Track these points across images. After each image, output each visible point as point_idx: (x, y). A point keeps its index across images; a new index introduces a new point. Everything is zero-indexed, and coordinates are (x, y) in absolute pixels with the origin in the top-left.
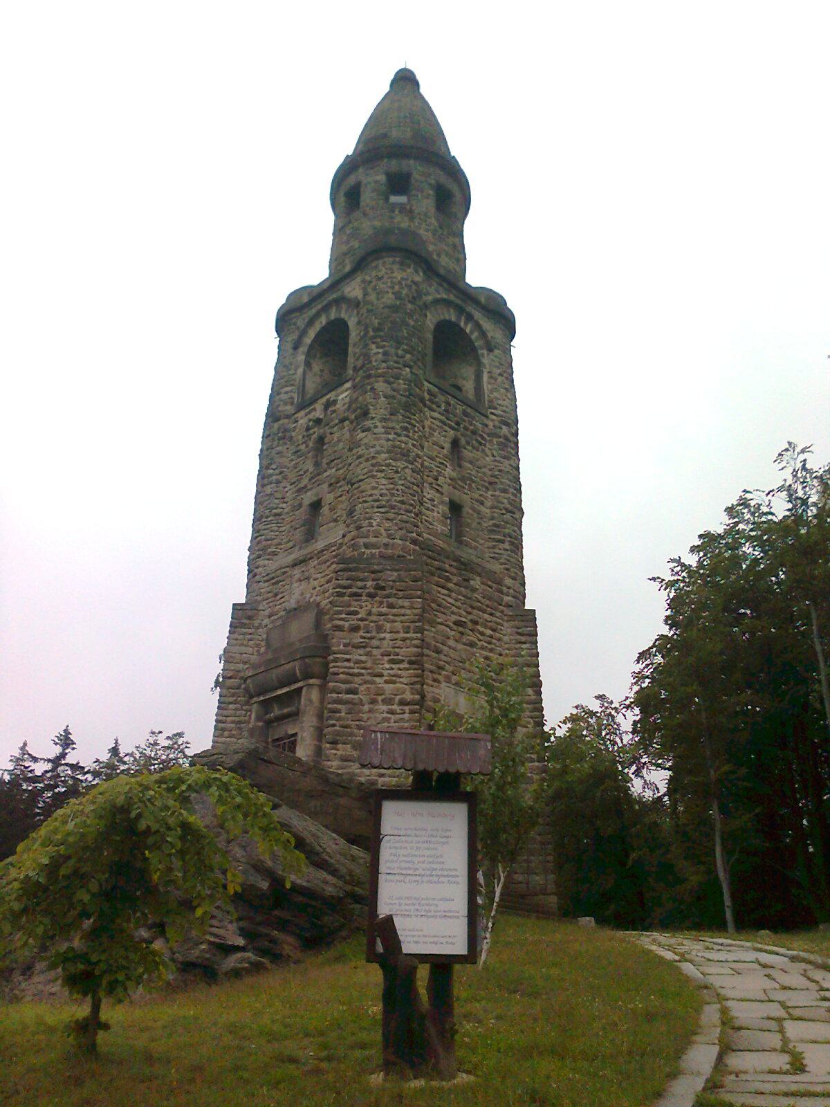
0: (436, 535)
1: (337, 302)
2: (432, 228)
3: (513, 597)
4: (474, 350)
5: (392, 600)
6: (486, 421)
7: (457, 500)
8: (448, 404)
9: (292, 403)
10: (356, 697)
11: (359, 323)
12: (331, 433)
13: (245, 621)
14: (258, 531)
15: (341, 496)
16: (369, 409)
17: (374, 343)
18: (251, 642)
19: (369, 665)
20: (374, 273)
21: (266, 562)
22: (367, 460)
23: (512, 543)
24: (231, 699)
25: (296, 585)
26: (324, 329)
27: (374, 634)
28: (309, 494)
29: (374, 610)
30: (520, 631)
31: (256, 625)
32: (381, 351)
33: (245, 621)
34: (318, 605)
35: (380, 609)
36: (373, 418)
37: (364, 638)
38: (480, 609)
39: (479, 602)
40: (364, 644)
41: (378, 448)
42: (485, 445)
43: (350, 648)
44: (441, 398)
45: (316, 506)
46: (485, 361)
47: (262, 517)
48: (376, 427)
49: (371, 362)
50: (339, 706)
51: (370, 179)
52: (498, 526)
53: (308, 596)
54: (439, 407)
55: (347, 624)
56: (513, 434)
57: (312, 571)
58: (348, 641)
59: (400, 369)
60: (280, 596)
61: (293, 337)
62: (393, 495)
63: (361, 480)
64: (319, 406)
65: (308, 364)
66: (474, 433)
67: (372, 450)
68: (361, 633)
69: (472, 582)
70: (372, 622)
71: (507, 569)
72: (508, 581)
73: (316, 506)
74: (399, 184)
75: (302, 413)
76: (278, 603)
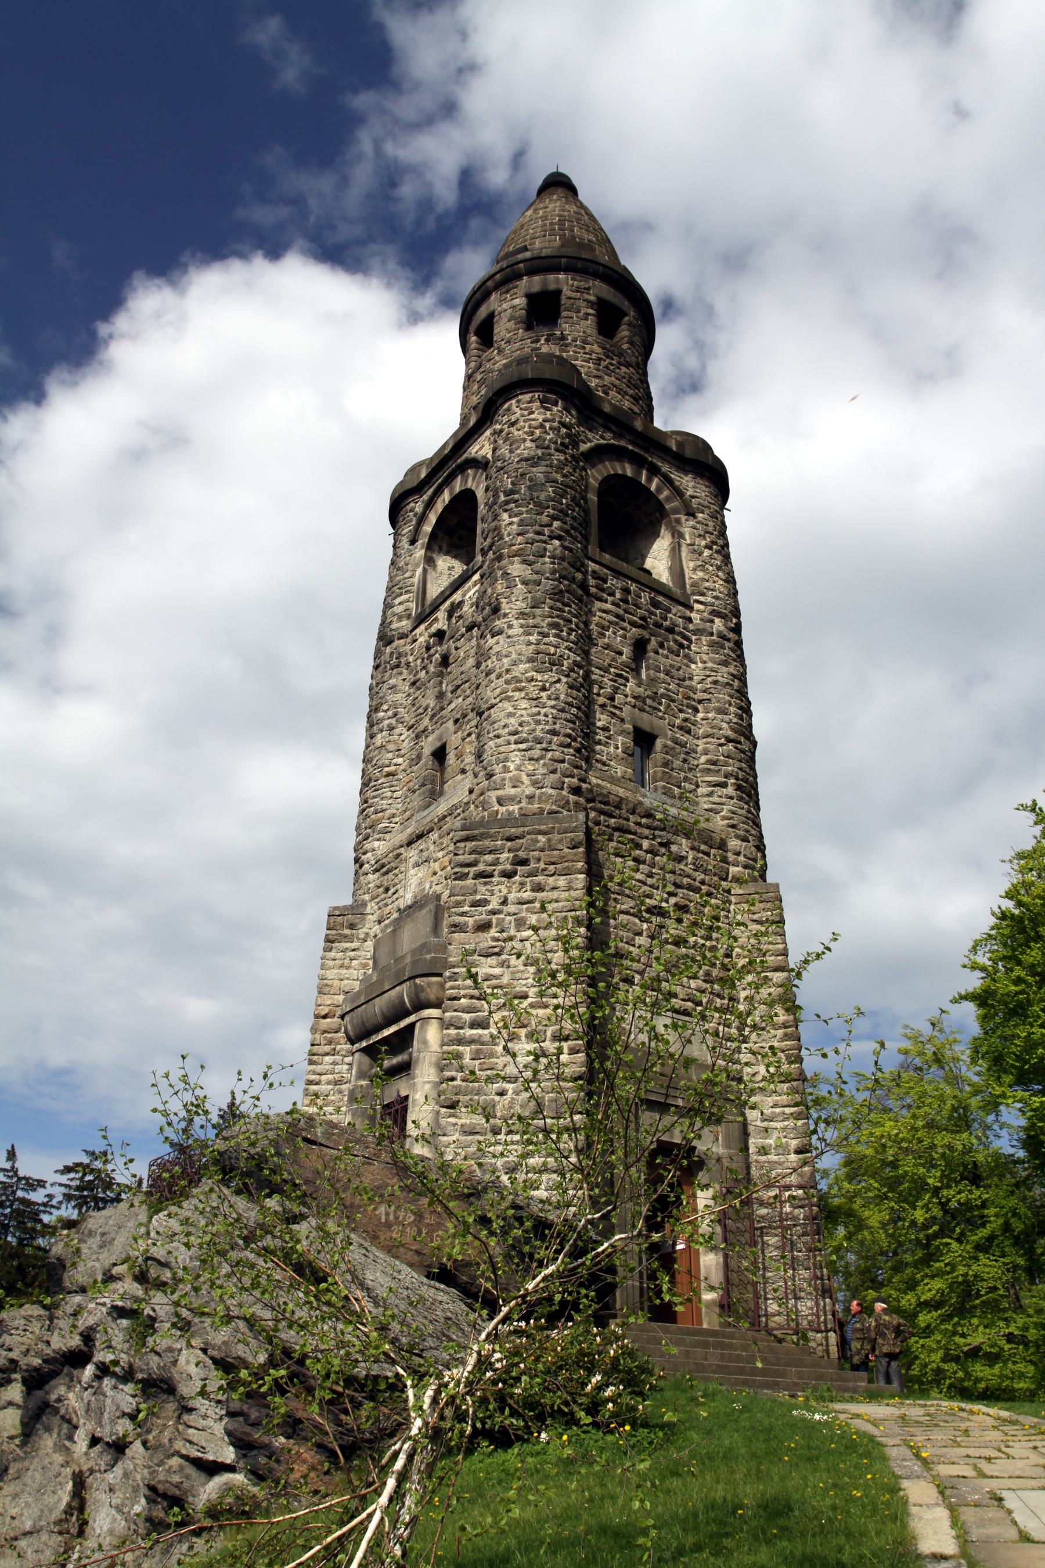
0: (613, 780)
1: (462, 469)
2: (594, 356)
3: (745, 867)
4: (660, 505)
5: (540, 878)
6: (688, 613)
7: (646, 727)
8: (626, 591)
9: (409, 616)
10: (486, 1032)
11: (487, 490)
12: (457, 649)
13: (347, 931)
14: (366, 802)
15: (469, 735)
16: (499, 603)
17: (506, 511)
18: (355, 963)
19: (505, 980)
20: (505, 419)
21: (376, 844)
22: (499, 676)
23: (739, 788)
24: (327, 1048)
25: (412, 872)
26: (446, 509)
27: (512, 932)
28: (430, 739)
29: (512, 897)
30: (755, 917)
31: (362, 936)
32: (515, 520)
33: (347, 931)
34: (438, 897)
35: (519, 895)
36: (505, 615)
37: (498, 940)
38: (690, 888)
39: (688, 876)
40: (497, 950)
41: (514, 656)
42: (689, 648)
43: (476, 957)
44: (612, 582)
45: (440, 754)
46: (687, 531)
47: (370, 780)
48: (510, 627)
49: (502, 538)
50: (461, 1048)
51: (505, 306)
52: (714, 763)
53: (428, 886)
54: (612, 594)
55: (471, 921)
56: (732, 630)
57: (432, 848)
58: (472, 947)
59: (545, 542)
60: (392, 891)
61: (407, 530)
62: (538, 723)
63: (492, 707)
64: (441, 614)
65: (430, 561)
66: (671, 630)
67: (505, 660)
68: (493, 932)
69: (674, 848)
70: (509, 914)
71: (733, 826)
72: (734, 844)
73: (440, 754)
74: (543, 311)
75: (422, 627)
76: (389, 901)
